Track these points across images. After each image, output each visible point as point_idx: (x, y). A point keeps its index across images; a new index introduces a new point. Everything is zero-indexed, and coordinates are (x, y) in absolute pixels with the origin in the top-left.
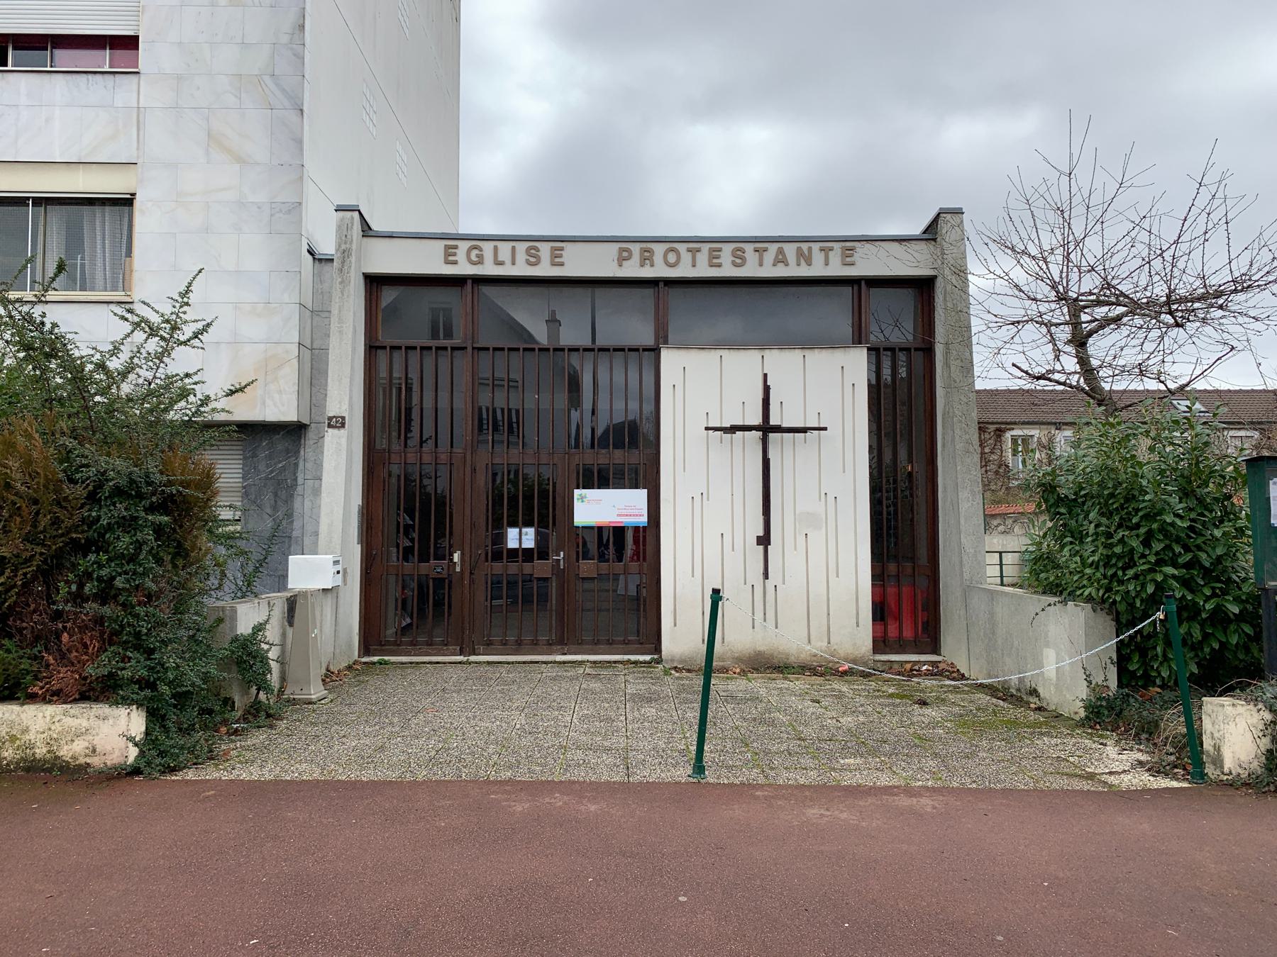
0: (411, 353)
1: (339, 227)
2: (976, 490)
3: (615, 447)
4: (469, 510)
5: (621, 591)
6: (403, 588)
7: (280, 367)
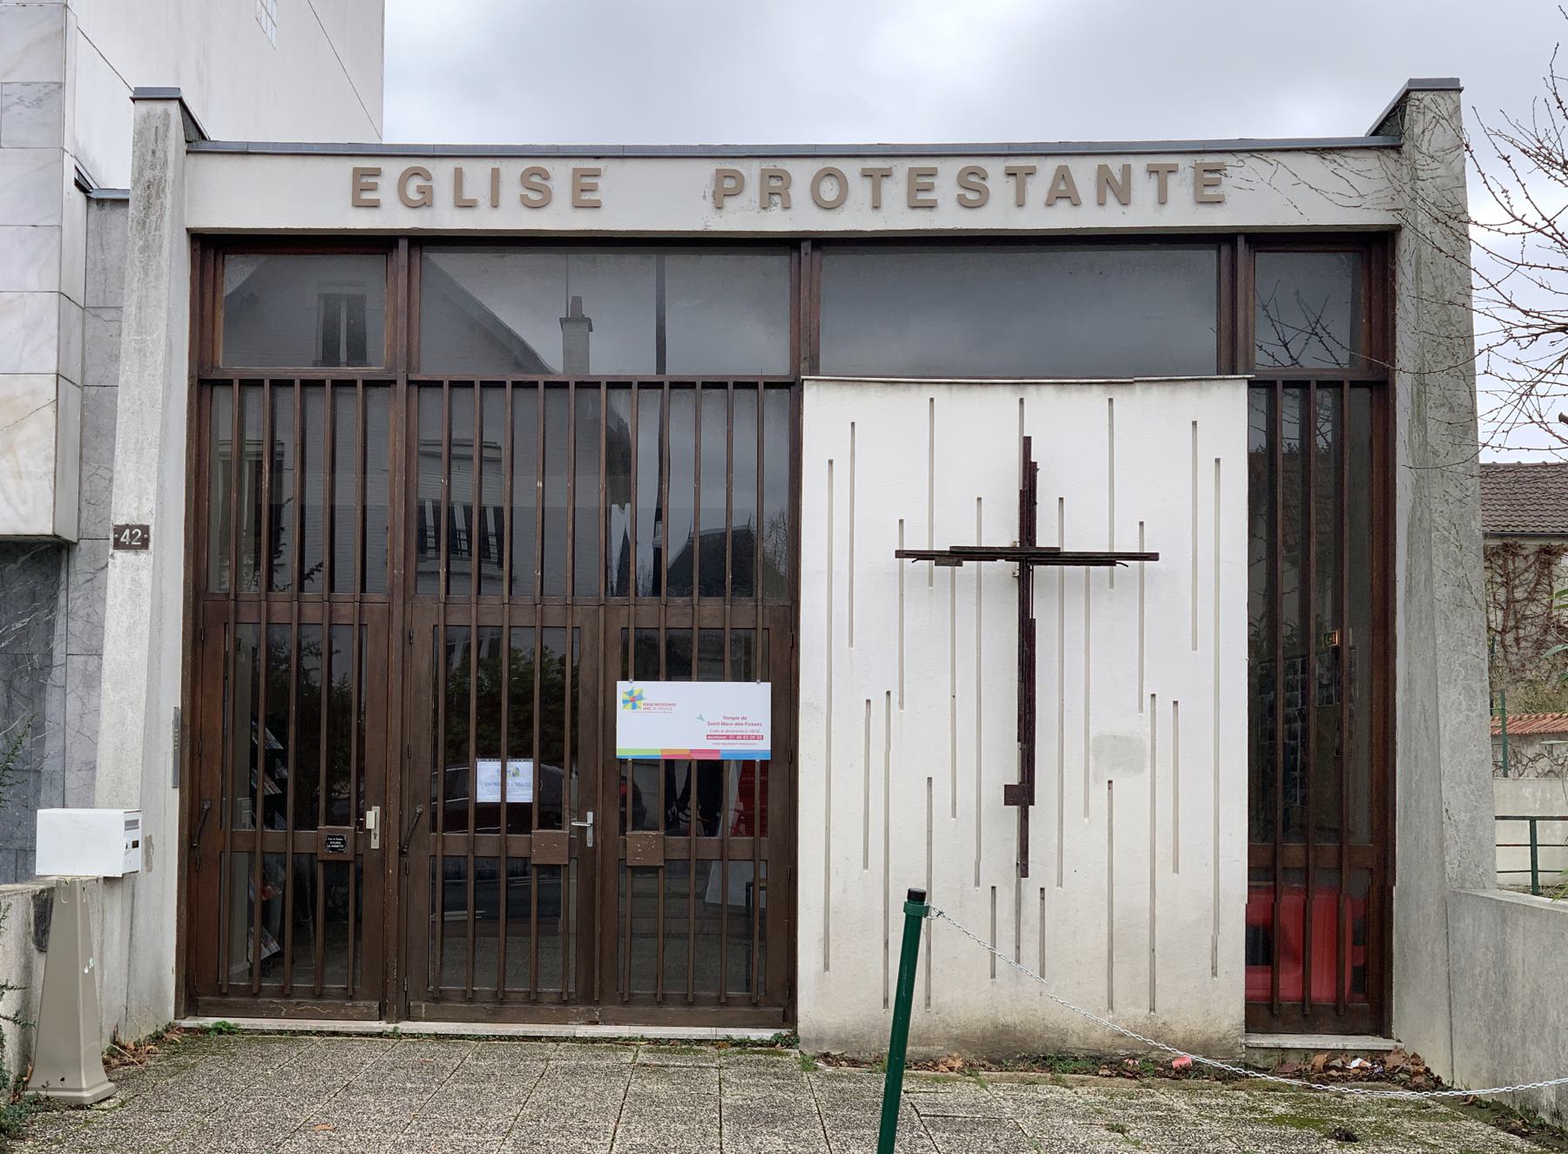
0: (282, 393)
1: (140, 135)
2: (1477, 686)
3: (707, 591)
4: (398, 721)
5: (712, 896)
6: (265, 881)
7: (17, 424)
